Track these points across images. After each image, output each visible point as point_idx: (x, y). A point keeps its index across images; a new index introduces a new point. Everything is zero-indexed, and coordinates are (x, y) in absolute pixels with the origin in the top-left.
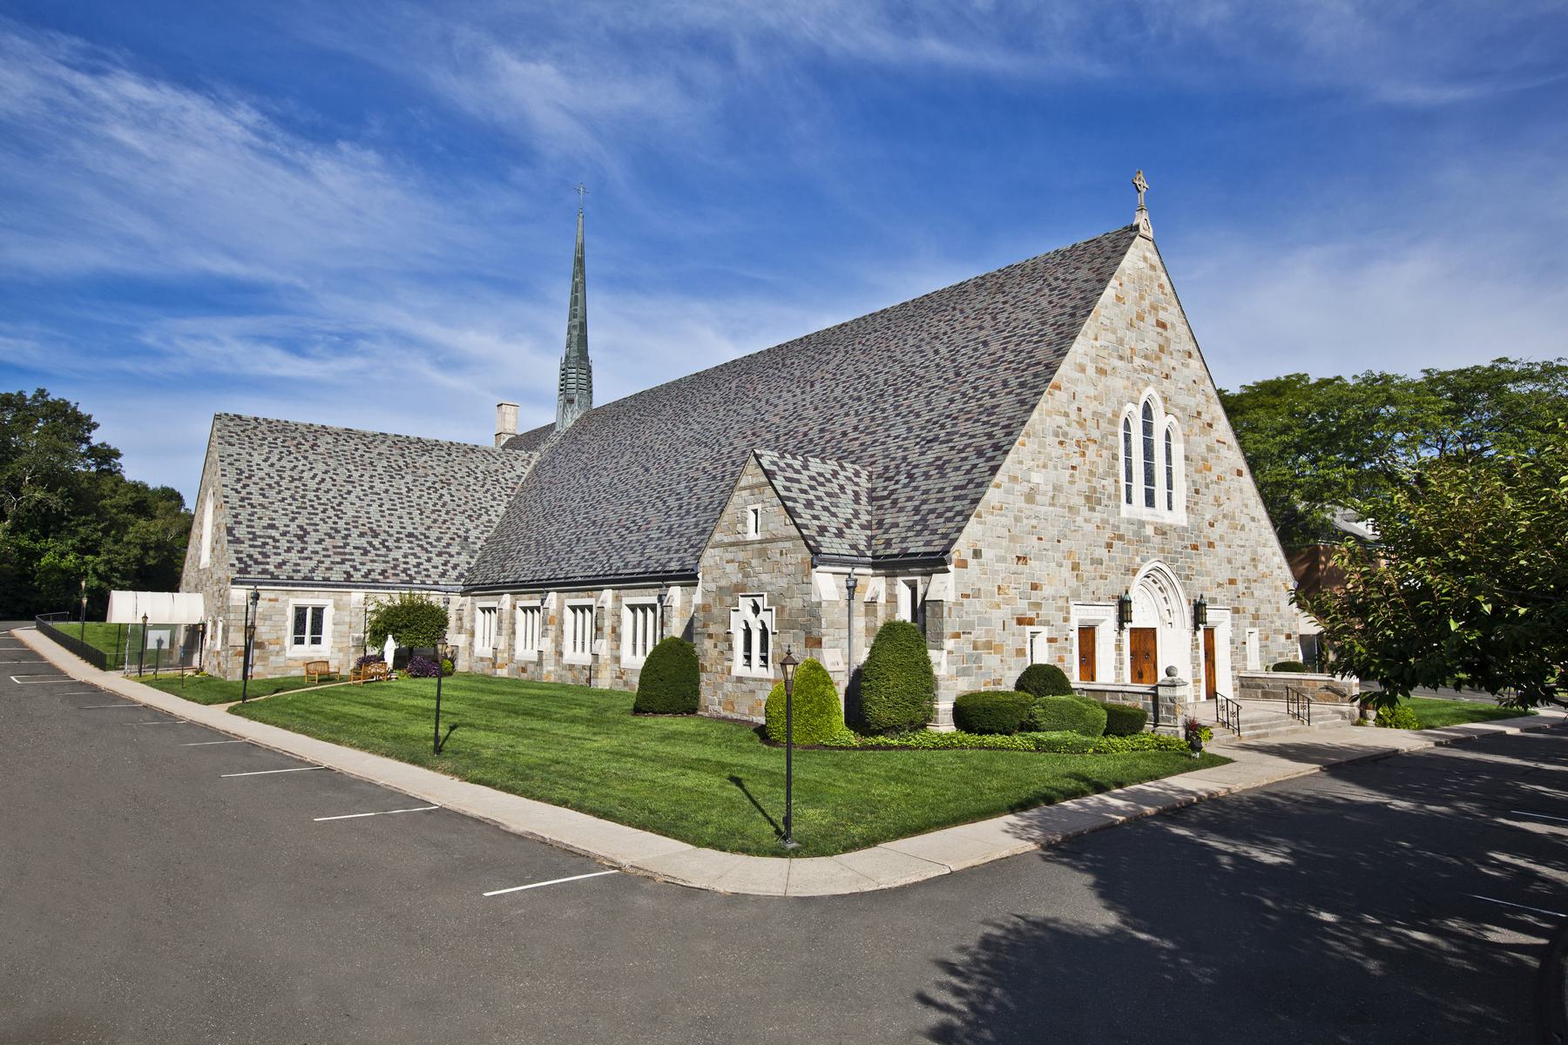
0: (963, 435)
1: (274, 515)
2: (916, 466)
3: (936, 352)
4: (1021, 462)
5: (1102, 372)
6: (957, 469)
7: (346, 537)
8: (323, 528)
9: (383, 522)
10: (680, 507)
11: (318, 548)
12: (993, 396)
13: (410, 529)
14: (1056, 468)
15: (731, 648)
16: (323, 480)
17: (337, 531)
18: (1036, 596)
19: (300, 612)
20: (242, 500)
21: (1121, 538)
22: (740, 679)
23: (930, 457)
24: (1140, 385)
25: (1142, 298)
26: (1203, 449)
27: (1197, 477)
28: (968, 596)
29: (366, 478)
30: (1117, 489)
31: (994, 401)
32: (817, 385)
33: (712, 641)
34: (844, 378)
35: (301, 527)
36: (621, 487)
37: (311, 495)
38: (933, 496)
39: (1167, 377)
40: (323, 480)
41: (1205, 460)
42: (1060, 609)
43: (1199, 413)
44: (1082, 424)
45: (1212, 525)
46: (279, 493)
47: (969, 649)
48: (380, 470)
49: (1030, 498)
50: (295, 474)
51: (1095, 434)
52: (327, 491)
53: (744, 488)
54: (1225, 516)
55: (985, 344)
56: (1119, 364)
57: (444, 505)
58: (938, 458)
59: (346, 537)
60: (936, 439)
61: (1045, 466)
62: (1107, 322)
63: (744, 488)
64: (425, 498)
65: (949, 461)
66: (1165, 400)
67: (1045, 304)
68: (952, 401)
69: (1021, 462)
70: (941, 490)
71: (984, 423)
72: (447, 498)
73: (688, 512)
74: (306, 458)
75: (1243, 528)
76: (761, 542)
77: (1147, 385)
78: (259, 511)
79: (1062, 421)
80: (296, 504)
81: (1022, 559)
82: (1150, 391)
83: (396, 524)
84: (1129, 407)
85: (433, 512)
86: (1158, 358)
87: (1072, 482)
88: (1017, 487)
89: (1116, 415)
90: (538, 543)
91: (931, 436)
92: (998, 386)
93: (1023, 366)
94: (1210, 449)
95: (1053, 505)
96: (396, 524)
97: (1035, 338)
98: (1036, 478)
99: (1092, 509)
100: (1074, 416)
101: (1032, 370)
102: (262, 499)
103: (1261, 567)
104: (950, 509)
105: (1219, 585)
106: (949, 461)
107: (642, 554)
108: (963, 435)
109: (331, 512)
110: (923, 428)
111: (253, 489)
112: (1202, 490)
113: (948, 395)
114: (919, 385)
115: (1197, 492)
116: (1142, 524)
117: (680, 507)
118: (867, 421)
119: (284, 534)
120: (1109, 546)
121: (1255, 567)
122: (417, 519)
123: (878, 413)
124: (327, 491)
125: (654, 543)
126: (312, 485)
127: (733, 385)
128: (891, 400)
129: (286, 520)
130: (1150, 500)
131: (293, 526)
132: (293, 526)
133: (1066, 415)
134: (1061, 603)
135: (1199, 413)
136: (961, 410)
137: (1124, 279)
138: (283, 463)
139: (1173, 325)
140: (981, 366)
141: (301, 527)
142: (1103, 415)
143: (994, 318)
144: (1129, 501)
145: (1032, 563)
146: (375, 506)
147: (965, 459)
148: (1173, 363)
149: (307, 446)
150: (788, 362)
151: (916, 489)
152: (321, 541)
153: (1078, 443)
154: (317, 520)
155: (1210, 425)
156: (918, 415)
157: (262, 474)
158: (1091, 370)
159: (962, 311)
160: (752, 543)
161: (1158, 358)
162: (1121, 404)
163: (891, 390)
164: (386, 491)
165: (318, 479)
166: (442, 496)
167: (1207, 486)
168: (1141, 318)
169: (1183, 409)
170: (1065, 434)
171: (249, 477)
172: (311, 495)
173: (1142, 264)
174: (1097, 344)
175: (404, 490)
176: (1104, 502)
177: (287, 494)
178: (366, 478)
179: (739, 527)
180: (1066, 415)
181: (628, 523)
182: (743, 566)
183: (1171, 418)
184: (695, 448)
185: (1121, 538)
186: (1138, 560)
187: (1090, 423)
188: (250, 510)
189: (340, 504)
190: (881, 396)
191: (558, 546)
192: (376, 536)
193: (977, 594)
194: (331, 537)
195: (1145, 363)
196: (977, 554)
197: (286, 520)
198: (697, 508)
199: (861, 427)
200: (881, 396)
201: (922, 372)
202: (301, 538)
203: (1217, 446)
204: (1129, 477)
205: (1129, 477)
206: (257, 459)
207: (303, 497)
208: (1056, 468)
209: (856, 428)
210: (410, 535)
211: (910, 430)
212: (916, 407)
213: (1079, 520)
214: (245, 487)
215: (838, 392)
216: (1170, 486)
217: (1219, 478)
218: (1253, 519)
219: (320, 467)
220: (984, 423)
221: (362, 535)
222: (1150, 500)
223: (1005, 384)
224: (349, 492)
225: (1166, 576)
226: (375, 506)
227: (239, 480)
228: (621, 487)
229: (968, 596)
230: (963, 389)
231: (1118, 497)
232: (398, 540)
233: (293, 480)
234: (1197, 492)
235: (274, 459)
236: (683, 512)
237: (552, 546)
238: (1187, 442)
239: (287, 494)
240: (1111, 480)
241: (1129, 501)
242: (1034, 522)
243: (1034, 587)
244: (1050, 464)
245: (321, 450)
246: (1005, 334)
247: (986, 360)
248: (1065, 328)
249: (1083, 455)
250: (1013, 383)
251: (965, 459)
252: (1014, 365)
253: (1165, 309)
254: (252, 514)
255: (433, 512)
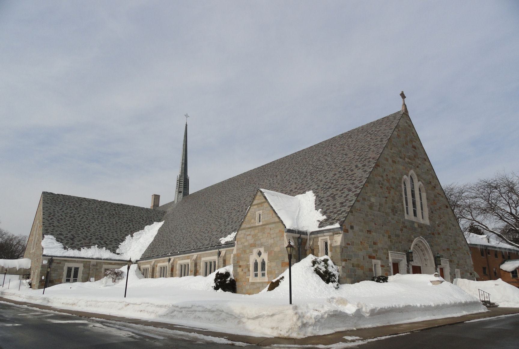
0: (341, 185)
1: (62, 230)
2: (323, 198)
3: (326, 160)
4: (366, 193)
5: (394, 162)
6: (340, 197)
7: (90, 239)
8: (82, 236)
9: (105, 234)
10: (225, 222)
11: (79, 243)
12: (352, 171)
13: (116, 237)
14: (380, 197)
15: (249, 270)
16: (83, 218)
17: (87, 237)
18: (375, 247)
19: (69, 269)
20: (50, 224)
21: (405, 227)
22: (253, 284)
23: (328, 194)
24: (409, 169)
25: (407, 137)
26: (433, 196)
27: (432, 207)
28: (349, 244)
29: (100, 217)
30: (403, 208)
31: (353, 173)
32: (279, 177)
33: (241, 269)
34: (289, 173)
35: (72, 235)
36: (201, 219)
37: (77, 223)
38: (331, 207)
39: (418, 167)
40: (83, 218)
41: (434, 200)
42: (385, 253)
43: (430, 182)
44: (388, 181)
45: (439, 226)
46: (65, 222)
47: (350, 266)
48: (106, 215)
49: (371, 206)
50: (72, 215)
51: (394, 186)
52: (84, 222)
53: (255, 205)
54: (443, 223)
55: (346, 155)
56: (400, 160)
57: (130, 229)
58: (332, 194)
59: (90, 239)
60: (330, 187)
61: (376, 195)
62: (395, 144)
63: (255, 205)
64: (123, 226)
65: (337, 194)
66: (418, 175)
67: (369, 139)
68: (335, 174)
69: (366, 193)
70: (335, 204)
71: (349, 180)
72: (131, 226)
73: (228, 224)
74: (76, 209)
75: (450, 229)
76: (262, 226)
77: (411, 169)
78: (56, 229)
79: (381, 179)
80: (71, 226)
81: (369, 232)
82: (412, 172)
83: (111, 235)
84: (405, 177)
85: (125, 231)
86: (414, 160)
87: (386, 203)
88: (366, 203)
89: (401, 179)
90: (167, 241)
91: (327, 187)
92: (354, 167)
93: (363, 160)
94: (435, 196)
95: (379, 211)
96: (111, 235)
97: (367, 150)
98: (373, 200)
99: (394, 215)
100: (385, 177)
101: (367, 160)
102: (58, 224)
103: (458, 245)
104: (340, 210)
105: (444, 250)
106: (337, 194)
107: (210, 240)
108: (341, 185)
109: (85, 230)
110: (324, 185)
111: (55, 220)
112: (434, 212)
113: (333, 173)
114: (320, 171)
115: (432, 212)
116: (413, 222)
117: (225, 222)
118: (300, 185)
119: (66, 237)
120: (402, 230)
121: (456, 244)
122: (119, 234)
123: (304, 182)
124: (84, 222)
125: (215, 236)
126: (78, 219)
127: (245, 181)
128: (309, 177)
129: (67, 232)
130: (415, 214)
131: (69, 235)
132: (69, 235)
133: (382, 177)
134: (385, 251)
135: (430, 182)
136: (339, 177)
137: (400, 129)
138: (67, 211)
139: (418, 148)
140: (345, 162)
141: (72, 235)
142: (396, 179)
143: (349, 146)
144: (407, 213)
145: (374, 234)
146: (103, 228)
147: (344, 193)
148: (419, 162)
149: (78, 205)
150: (266, 171)
151: (324, 205)
152: (80, 241)
153: (387, 188)
154: (79, 232)
155: (435, 187)
156: (321, 181)
157: (59, 214)
158: (390, 161)
159: (335, 146)
160: (258, 226)
161: (414, 160)
162: (402, 175)
163: (309, 174)
164: (108, 223)
165: (80, 217)
166: (129, 225)
167: (436, 211)
168: (407, 144)
169: (424, 180)
170: (382, 184)
171: (54, 216)
172: (77, 223)
173: (406, 125)
174: (392, 151)
175: (115, 223)
176: (399, 213)
177: (68, 222)
178: (100, 217)
179: (253, 221)
180: (382, 177)
181: (204, 231)
182: (254, 236)
183: (420, 183)
184: (231, 203)
185: (405, 227)
186: (413, 237)
187: (391, 181)
188: (52, 228)
189: (89, 227)
190: (305, 177)
191: (175, 241)
192: (102, 239)
193: (353, 244)
194: (84, 239)
195: (409, 161)
196: (352, 227)
197: (67, 232)
198: (232, 222)
199: (298, 188)
200: (305, 177)
201: (321, 167)
202: (72, 239)
203: (438, 195)
204: (407, 204)
205: (407, 204)
206: (57, 209)
207: (74, 224)
208: (380, 197)
209: (296, 188)
210: (116, 240)
211: (318, 186)
212: (320, 178)
213: (390, 218)
214: (51, 219)
215: (287, 177)
216: (422, 209)
217: (440, 208)
218: (453, 225)
219: (83, 213)
220: (349, 180)
221: (97, 239)
222: (415, 214)
223: (357, 166)
224: (93, 223)
225: (424, 245)
226: (103, 228)
227: (49, 217)
228: (201, 219)
229: (349, 244)
230: (339, 170)
231: (404, 211)
232: (111, 241)
233: (71, 217)
234: (432, 212)
235: (64, 209)
236: (226, 224)
237: (173, 242)
238: (427, 193)
239: (68, 222)
240: (399, 204)
241: (407, 213)
242: (373, 217)
243: (375, 243)
244: (378, 195)
245: (83, 207)
246: (354, 151)
247: (347, 160)
248: (379, 146)
249: (389, 193)
250: (360, 165)
251: (344, 193)
252: (359, 160)
253: (415, 142)
254: (53, 230)
255: (125, 231)
